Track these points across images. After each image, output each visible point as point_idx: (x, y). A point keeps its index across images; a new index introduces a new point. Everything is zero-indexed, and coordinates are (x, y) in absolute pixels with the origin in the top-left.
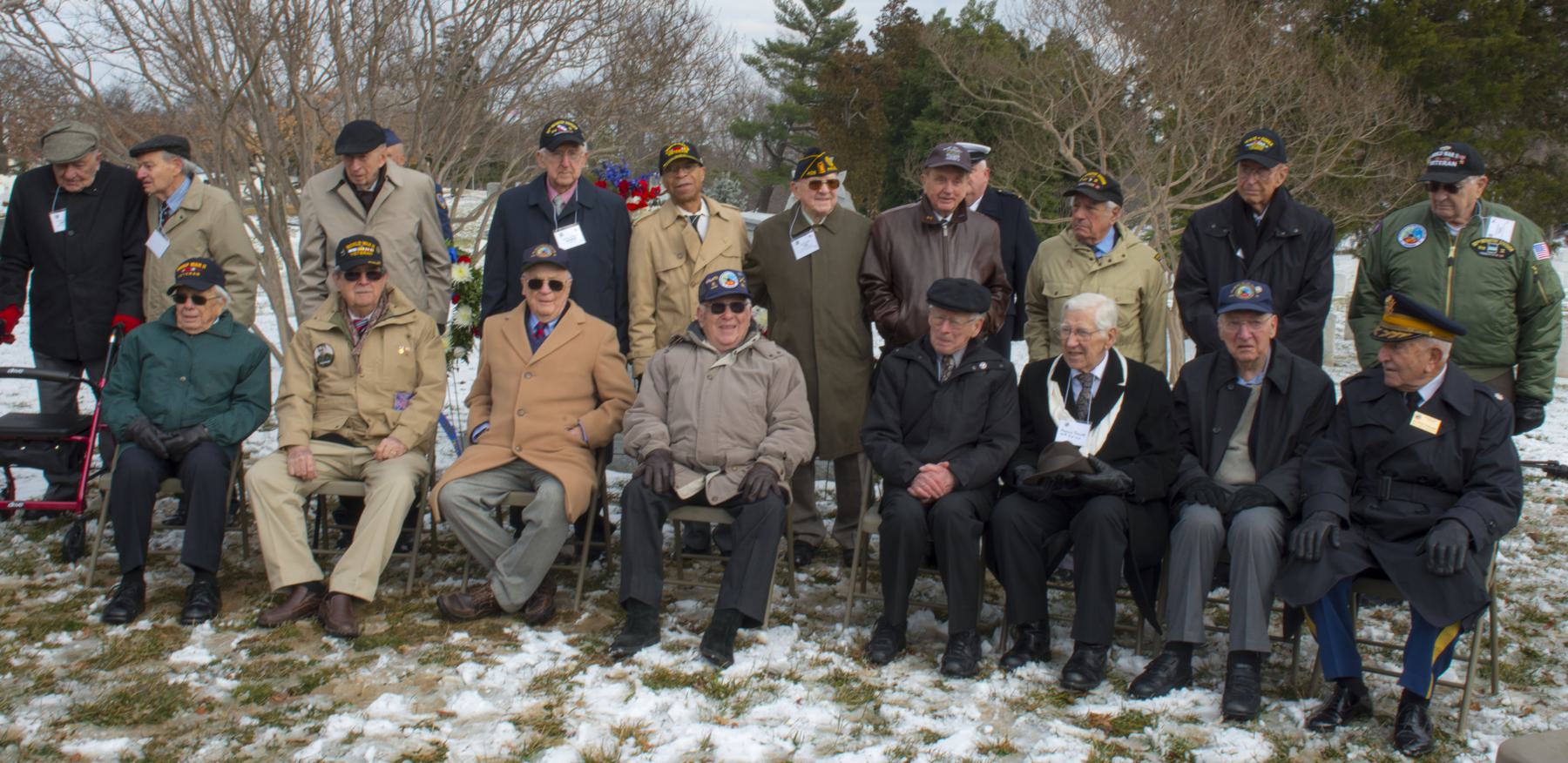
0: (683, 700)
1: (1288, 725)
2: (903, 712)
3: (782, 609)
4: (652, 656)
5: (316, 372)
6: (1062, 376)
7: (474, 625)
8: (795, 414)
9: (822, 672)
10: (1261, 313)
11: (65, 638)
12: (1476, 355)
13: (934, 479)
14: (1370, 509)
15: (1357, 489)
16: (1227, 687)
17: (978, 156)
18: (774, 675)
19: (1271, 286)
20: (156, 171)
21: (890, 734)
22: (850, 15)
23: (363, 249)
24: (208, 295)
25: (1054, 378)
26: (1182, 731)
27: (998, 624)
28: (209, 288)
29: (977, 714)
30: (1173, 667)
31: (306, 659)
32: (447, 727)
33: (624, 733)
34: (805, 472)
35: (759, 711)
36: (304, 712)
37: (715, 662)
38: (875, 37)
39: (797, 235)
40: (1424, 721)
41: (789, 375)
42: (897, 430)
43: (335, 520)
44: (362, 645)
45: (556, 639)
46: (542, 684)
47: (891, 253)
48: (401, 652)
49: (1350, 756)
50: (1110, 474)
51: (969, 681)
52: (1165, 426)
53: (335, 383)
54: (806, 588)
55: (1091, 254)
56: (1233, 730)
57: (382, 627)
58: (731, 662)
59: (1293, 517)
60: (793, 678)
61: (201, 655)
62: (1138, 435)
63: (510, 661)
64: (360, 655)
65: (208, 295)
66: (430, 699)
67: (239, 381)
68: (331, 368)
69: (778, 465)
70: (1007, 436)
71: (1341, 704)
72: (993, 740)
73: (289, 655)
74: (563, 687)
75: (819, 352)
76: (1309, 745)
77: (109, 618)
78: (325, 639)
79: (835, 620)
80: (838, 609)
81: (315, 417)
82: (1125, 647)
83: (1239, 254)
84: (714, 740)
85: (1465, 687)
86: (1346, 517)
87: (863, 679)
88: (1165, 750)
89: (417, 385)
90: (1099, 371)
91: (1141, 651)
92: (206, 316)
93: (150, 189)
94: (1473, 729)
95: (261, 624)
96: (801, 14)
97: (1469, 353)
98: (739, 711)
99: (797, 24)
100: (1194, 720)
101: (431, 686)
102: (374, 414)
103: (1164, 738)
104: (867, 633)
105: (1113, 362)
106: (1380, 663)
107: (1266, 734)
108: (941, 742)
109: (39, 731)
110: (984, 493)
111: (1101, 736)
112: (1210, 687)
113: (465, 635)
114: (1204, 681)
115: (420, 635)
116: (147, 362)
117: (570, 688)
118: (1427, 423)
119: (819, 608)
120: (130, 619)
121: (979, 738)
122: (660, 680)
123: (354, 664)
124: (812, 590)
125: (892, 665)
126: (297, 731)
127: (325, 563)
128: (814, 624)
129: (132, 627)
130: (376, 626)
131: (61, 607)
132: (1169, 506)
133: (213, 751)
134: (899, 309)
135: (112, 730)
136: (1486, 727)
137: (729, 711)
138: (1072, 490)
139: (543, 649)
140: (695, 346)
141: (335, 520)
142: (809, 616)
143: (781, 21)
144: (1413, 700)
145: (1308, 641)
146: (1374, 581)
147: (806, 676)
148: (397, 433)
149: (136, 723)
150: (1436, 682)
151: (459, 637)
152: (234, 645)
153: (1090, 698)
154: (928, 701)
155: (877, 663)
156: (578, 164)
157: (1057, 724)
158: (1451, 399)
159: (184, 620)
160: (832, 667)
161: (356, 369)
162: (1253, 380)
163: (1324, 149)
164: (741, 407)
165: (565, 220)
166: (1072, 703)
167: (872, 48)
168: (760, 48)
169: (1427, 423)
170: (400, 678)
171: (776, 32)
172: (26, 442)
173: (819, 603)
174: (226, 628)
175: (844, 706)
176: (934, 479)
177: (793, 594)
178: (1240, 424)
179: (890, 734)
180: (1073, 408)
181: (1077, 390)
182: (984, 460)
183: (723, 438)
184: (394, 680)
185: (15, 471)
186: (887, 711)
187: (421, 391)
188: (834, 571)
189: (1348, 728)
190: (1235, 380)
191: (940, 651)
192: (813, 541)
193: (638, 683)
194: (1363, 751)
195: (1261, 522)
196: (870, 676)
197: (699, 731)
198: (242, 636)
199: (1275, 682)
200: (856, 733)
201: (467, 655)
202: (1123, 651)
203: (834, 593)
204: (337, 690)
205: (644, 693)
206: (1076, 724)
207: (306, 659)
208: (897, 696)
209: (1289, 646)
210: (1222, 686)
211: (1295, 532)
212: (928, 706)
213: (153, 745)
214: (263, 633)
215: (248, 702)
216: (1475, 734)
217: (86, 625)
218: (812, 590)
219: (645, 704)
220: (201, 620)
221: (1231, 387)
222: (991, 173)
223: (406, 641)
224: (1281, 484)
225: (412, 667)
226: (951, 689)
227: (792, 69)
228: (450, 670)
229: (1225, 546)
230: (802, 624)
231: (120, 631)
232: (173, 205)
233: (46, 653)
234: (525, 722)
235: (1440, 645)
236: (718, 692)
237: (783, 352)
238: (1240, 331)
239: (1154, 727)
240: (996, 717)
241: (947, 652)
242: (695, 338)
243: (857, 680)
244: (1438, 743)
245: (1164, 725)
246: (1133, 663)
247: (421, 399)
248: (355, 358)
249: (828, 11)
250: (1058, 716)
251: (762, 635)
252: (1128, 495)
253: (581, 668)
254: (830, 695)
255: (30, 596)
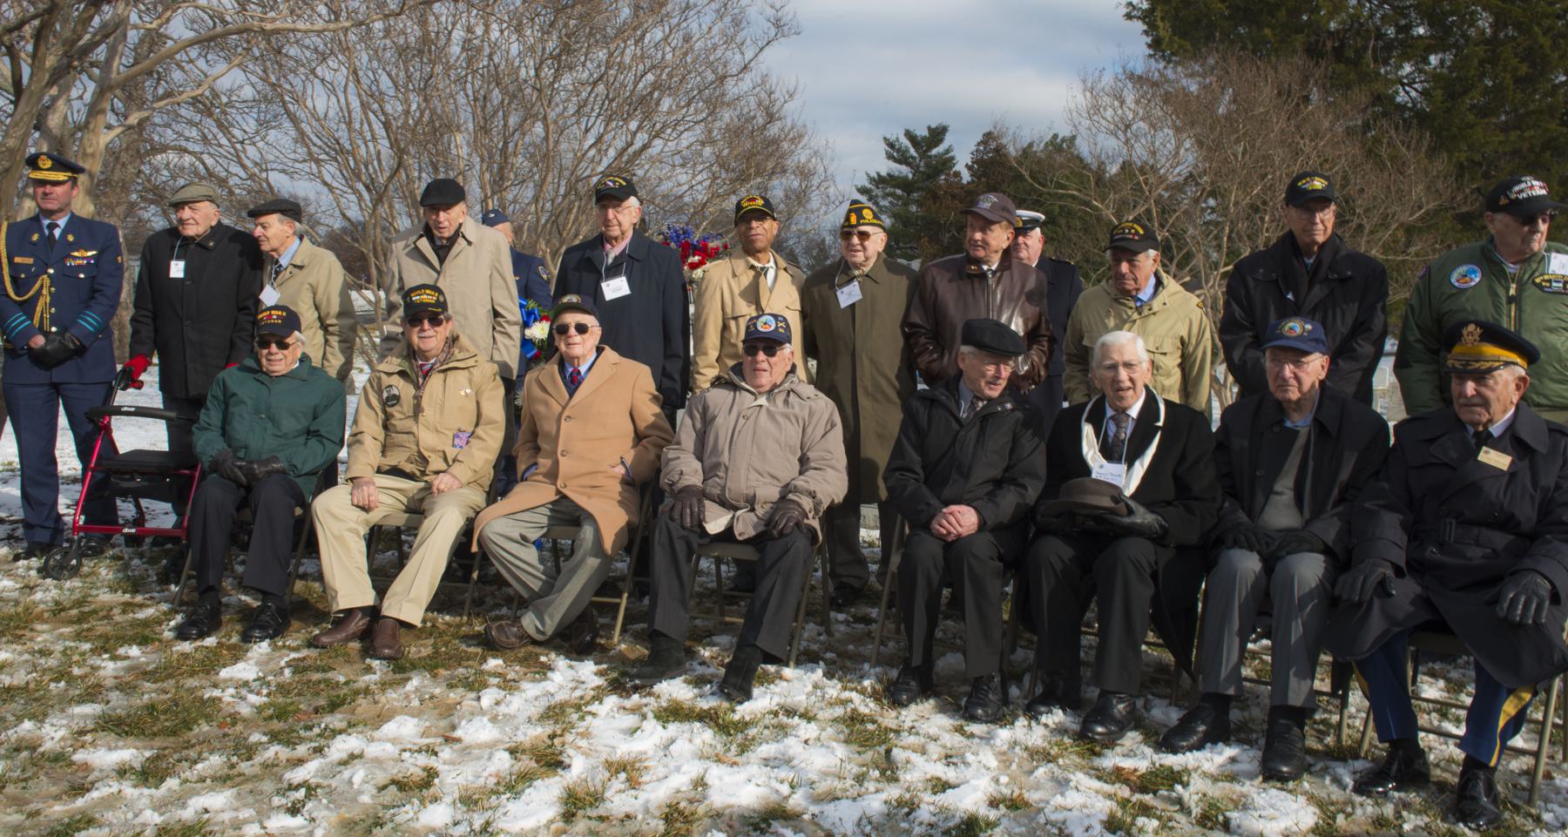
0: (687, 735)
1: (1334, 788)
2: (915, 757)
3: (815, 647)
4: (675, 689)
5: (385, 412)
6: (1097, 420)
7: (510, 654)
8: (828, 456)
9: (839, 711)
10: (1307, 353)
11: (134, 651)
12: (1546, 397)
13: (963, 519)
14: (1432, 552)
15: (1416, 533)
16: (1267, 743)
17: (1034, 222)
18: (790, 712)
19: (1324, 324)
20: (270, 233)
21: (897, 780)
22: (947, 151)
23: (427, 297)
24: (289, 340)
25: (1087, 420)
26: (1217, 791)
27: (1029, 669)
28: (289, 335)
29: (993, 763)
30: (1212, 718)
31: (342, 679)
32: (446, 753)
33: (618, 767)
34: (841, 517)
35: (766, 750)
36: (316, 730)
37: (729, 698)
38: (969, 168)
39: (841, 286)
40: (1490, 788)
41: (826, 417)
42: (920, 471)
43: (388, 549)
44: (401, 667)
45: (588, 670)
46: (554, 712)
47: (936, 301)
48: (435, 676)
49: (1406, 827)
50: (1143, 517)
51: (992, 726)
52: (1207, 465)
53: (399, 422)
54: (842, 628)
55: (1132, 304)
56: (1274, 792)
57: (426, 651)
58: (748, 696)
59: (1340, 561)
60: (808, 717)
61: (250, 672)
62: (1177, 478)
63: (531, 689)
64: (398, 676)
65: (289, 340)
66: (444, 723)
67: (315, 418)
68: (398, 407)
69: (807, 503)
70: (1035, 476)
71: (1395, 767)
72: (1006, 791)
73: (330, 675)
74: (575, 717)
75: (863, 401)
76: (1359, 811)
77: (182, 634)
78: (368, 661)
79: (865, 659)
80: (869, 649)
81: (384, 453)
82: (1159, 696)
83: (1290, 296)
84: (709, 779)
85: (1536, 755)
86: (1403, 564)
87: (880, 720)
88: (1196, 811)
89: (477, 425)
90: (1134, 412)
91: (1175, 702)
92: (290, 359)
93: (265, 247)
94: (1547, 800)
95: (312, 643)
96: (907, 150)
97: (1538, 393)
98: (743, 749)
99: (903, 159)
100: (1232, 778)
101: (449, 710)
102: (434, 451)
103: (1195, 798)
104: (894, 673)
105: (1151, 400)
106: (1436, 723)
107: (1311, 798)
108: (949, 791)
109: (63, 739)
110: (1015, 539)
111: (1125, 792)
112: (1249, 743)
113: (500, 662)
114: (1243, 736)
115: (460, 659)
116: (232, 401)
117: (582, 718)
118: (1497, 459)
119: (851, 647)
120: (202, 635)
121: (991, 789)
122: (674, 713)
123: (384, 685)
124: (848, 630)
125: (913, 707)
126: (302, 750)
127: (381, 591)
128: (841, 665)
129: (198, 643)
130: (419, 650)
131: (146, 623)
132: (1203, 556)
133: (211, 767)
134: (941, 357)
135: (130, 740)
136: (1560, 798)
137: (734, 748)
138: (1099, 530)
139: (571, 676)
140: (735, 387)
141: (388, 549)
142: (839, 655)
143: (890, 157)
144: (1475, 766)
145: (1356, 698)
146: (1433, 636)
147: (821, 715)
148: (456, 469)
149: (155, 734)
150: (1504, 747)
151: (494, 663)
152: (283, 663)
153: (1118, 749)
154: (944, 747)
155: (897, 704)
156: (627, 215)
157: (1080, 778)
158: (1525, 435)
159: (247, 638)
160: (850, 707)
161: (418, 409)
162: (1300, 422)
163: (1372, 232)
164: (780, 445)
165: (613, 271)
166: (1099, 755)
167: (966, 177)
168: (872, 180)
169: (1497, 459)
170: (422, 701)
171: (886, 167)
172: (142, 474)
173: (853, 642)
174: (284, 646)
175: (855, 747)
176: (963, 519)
177: (829, 633)
178: (1286, 467)
179: (897, 780)
180: (1109, 452)
181: (1112, 429)
182: (1009, 501)
183: (753, 476)
184: (416, 703)
185: (144, 502)
186: (898, 754)
187: (479, 431)
188: (874, 613)
189: (1402, 795)
190: (1283, 421)
191: (965, 694)
192: (856, 584)
193: (650, 715)
194: (1422, 820)
195: (1309, 569)
196: (889, 718)
197: (693, 769)
198: (293, 655)
199: (1321, 741)
200: (860, 779)
201: (494, 681)
202: (1157, 701)
203: (869, 634)
204: (359, 710)
205: (651, 724)
206: (1099, 778)
207: (342, 679)
208: (912, 739)
209: (1337, 702)
210: (1262, 742)
211: (1341, 579)
212: (943, 752)
213: (157, 758)
214: (313, 653)
215: (271, 718)
216: (1550, 806)
217: (160, 641)
218: (848, 630)
219: (653, 734)
220: (262, 639)
221: (1276, 429)
222: (1048, 240)
223: (443, 666)
224: (1329, 529)
225: (437, 691)
226: (972, 736)
227: (899, 198)
228: (473, 695)
229: (1267, 594)
230: (828, 663)
231: (186, 647)
232: (284, 262)
233: (111, 665)
234: (524, 752)
235: (1509, 708)
236: (725, 728)
237: (821, 395)
238: (1282, 369)
239: (1185, 785)
240: (1014, 766)
241: (970, 696)
242: (735, 379)
243: (874, 722)
244: (1507, 815)
245: (1197, 784)
246: (1166, 714)
247: (479, 438)
248: (418, 398)
249: (930, 148)
250: (1081, 769)
251: (788, 672)
252: (1158, 538)
253: (598, 698)
254: (842, 737)
255: (124, 612)
